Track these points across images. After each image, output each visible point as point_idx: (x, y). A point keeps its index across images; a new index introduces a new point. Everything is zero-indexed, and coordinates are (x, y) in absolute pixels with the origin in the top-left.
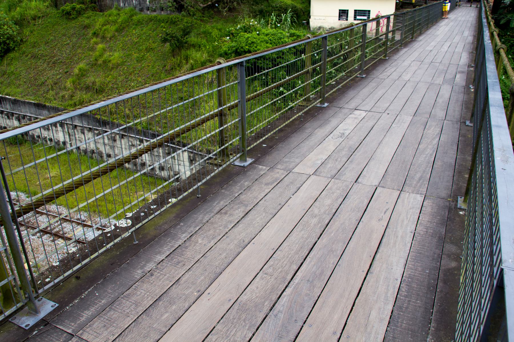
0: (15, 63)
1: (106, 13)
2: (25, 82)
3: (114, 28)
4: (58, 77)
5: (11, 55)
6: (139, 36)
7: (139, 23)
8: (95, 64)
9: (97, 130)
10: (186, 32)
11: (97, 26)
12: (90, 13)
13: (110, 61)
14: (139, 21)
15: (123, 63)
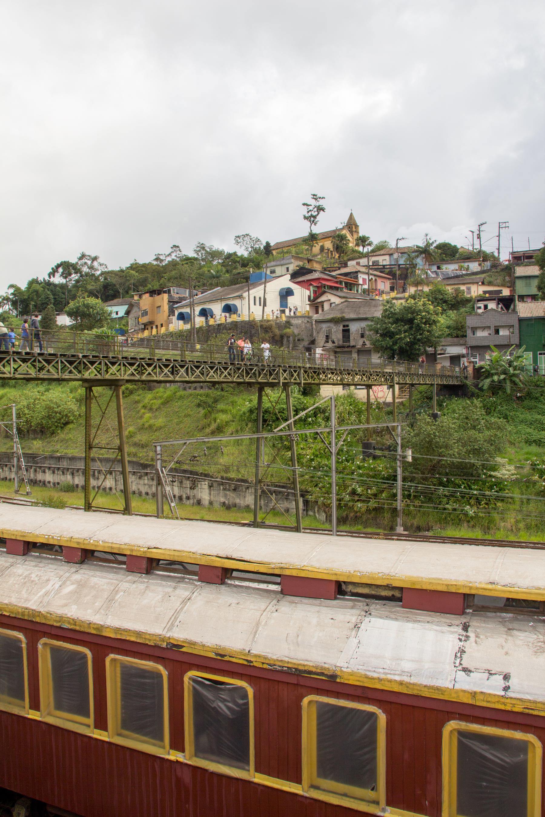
0: (73, 432)
1: (154, 391)
2: (81, 445)
3: (160, 401)
4: (110, 439)
5: (71, 426)
6: (180, 407)
7: (181, 397)
8: (142, 428)
9: (140, 472)
10: (216, 401)
11: (146, 401)
12: (141, 392)
13: (154, 425)
14: (181, 396)
15: (165, 426)
